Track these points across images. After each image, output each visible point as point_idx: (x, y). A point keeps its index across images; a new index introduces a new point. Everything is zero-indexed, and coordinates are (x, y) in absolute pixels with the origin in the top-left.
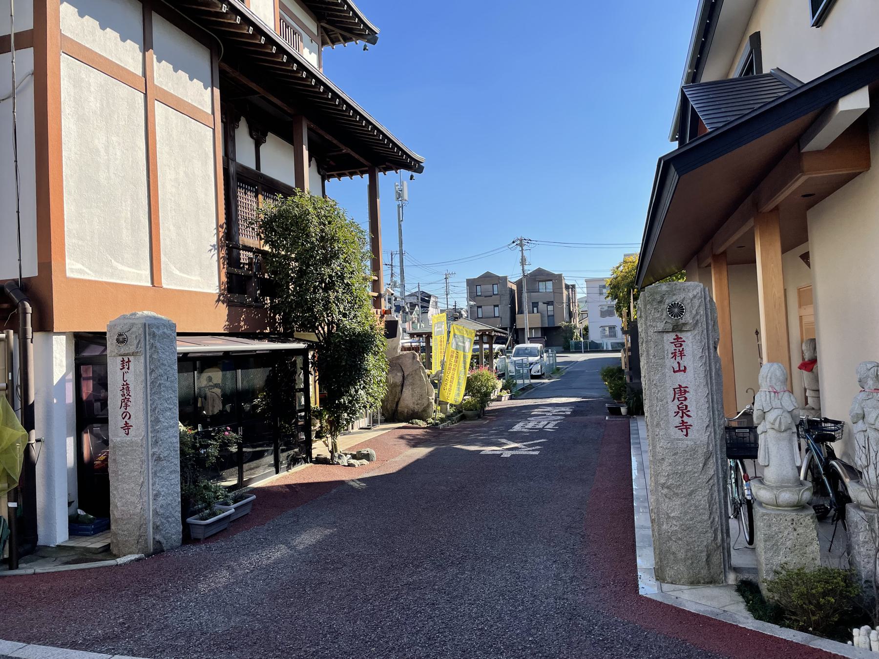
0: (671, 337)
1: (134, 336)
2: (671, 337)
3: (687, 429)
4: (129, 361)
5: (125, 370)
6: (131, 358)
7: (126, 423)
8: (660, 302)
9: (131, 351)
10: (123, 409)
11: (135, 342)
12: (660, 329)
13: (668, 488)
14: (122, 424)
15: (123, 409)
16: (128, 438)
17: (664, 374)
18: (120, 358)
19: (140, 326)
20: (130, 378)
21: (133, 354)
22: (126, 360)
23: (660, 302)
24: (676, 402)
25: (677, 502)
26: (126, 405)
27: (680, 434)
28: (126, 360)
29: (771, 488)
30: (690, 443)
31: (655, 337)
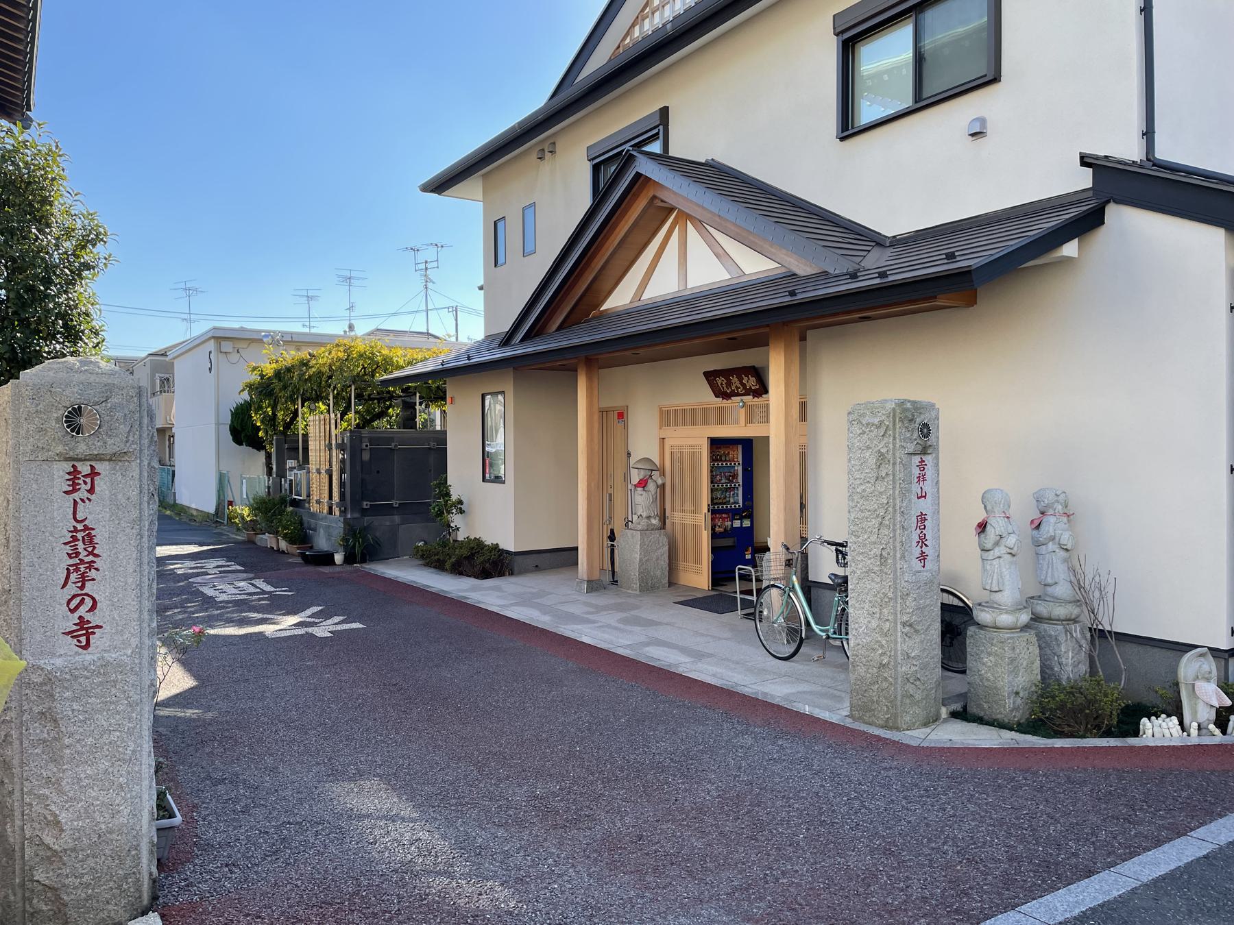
0: (916, 460)
1: (119, 415)
2: (916, 460)
3: (88, 635)
4: (94, 474)
5: (83, 493)
6: (99, 467)
7: (923, 553)
8: (911, 420)
9: (110, 450)
10: (72, 589)
11: (124, 428)
12: (911, 451)
13: (910, 625)
14: (71, 622)
15: (72, 589)
16: (88, 657)
17: (910, 500)
18: (68, 467)
19: (132, 392)
20: (95, 513)
21: (113, 458)
22: (84, 469)
23: (911, 420)
24: (918, 531)
25: (918, 639)
26: (83, 580)
27: (917, 565)
28: (84, 469)
29: (1008, 612)
30: (929, 575)
31: (905, 459)
